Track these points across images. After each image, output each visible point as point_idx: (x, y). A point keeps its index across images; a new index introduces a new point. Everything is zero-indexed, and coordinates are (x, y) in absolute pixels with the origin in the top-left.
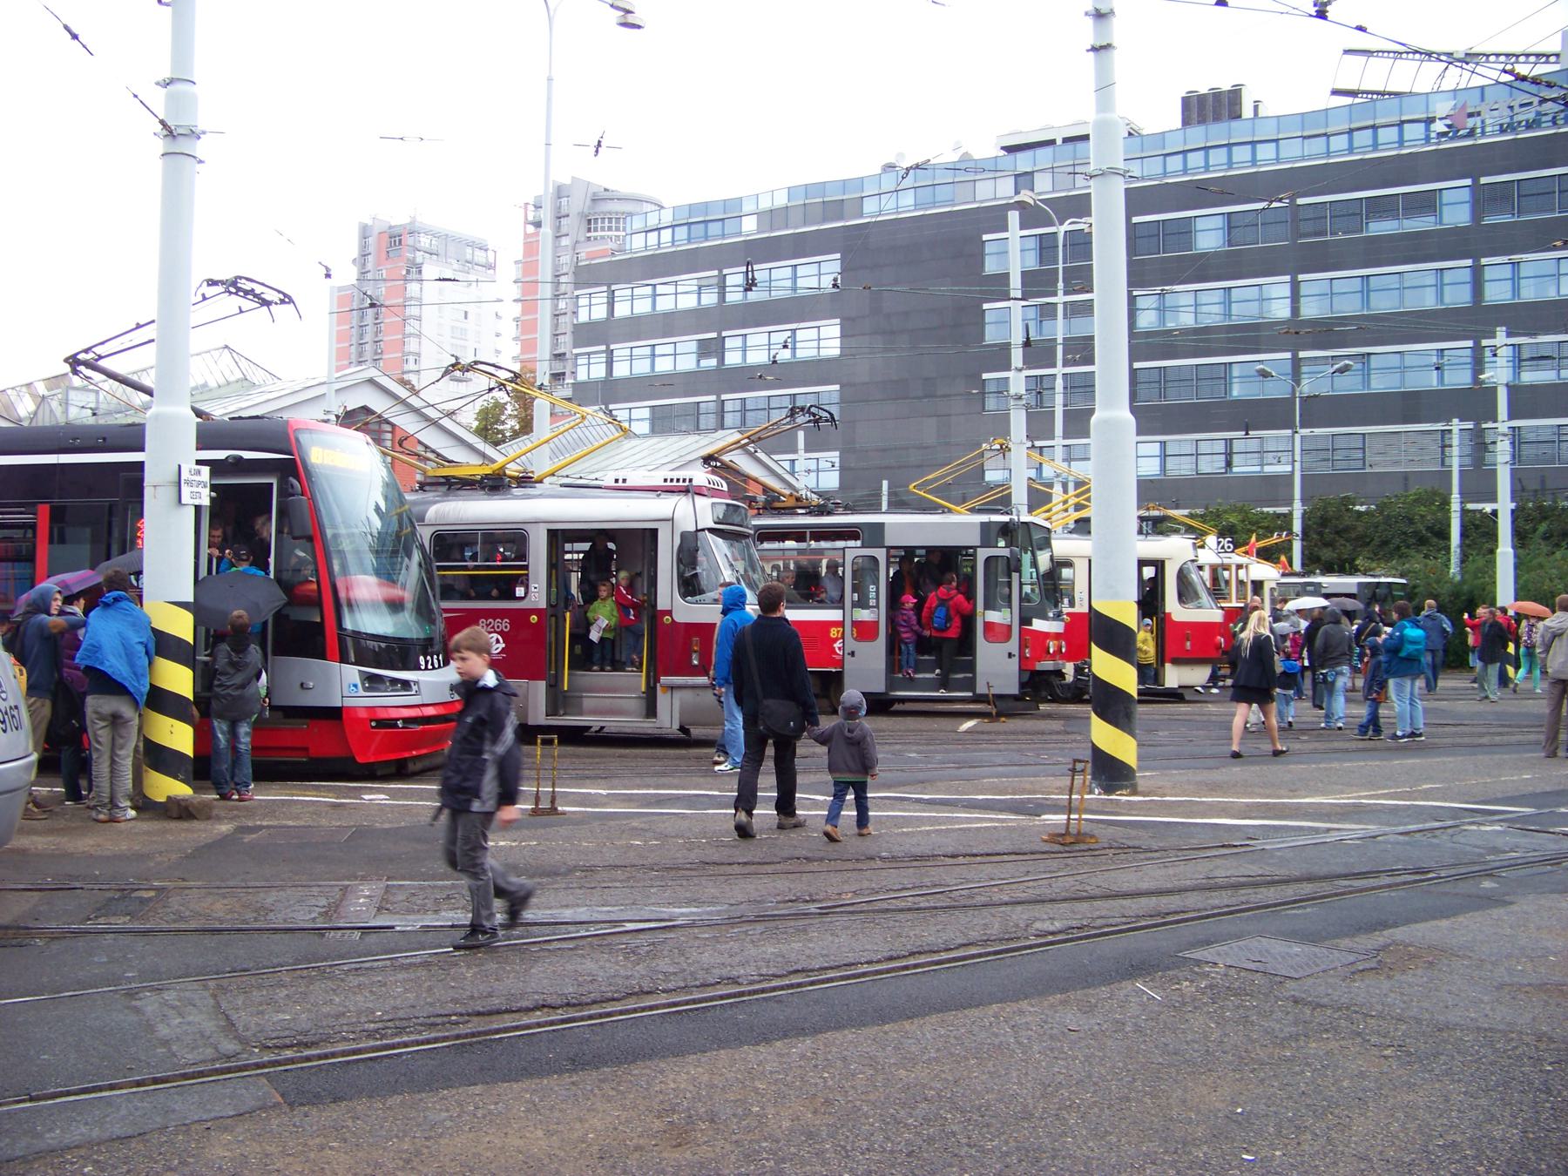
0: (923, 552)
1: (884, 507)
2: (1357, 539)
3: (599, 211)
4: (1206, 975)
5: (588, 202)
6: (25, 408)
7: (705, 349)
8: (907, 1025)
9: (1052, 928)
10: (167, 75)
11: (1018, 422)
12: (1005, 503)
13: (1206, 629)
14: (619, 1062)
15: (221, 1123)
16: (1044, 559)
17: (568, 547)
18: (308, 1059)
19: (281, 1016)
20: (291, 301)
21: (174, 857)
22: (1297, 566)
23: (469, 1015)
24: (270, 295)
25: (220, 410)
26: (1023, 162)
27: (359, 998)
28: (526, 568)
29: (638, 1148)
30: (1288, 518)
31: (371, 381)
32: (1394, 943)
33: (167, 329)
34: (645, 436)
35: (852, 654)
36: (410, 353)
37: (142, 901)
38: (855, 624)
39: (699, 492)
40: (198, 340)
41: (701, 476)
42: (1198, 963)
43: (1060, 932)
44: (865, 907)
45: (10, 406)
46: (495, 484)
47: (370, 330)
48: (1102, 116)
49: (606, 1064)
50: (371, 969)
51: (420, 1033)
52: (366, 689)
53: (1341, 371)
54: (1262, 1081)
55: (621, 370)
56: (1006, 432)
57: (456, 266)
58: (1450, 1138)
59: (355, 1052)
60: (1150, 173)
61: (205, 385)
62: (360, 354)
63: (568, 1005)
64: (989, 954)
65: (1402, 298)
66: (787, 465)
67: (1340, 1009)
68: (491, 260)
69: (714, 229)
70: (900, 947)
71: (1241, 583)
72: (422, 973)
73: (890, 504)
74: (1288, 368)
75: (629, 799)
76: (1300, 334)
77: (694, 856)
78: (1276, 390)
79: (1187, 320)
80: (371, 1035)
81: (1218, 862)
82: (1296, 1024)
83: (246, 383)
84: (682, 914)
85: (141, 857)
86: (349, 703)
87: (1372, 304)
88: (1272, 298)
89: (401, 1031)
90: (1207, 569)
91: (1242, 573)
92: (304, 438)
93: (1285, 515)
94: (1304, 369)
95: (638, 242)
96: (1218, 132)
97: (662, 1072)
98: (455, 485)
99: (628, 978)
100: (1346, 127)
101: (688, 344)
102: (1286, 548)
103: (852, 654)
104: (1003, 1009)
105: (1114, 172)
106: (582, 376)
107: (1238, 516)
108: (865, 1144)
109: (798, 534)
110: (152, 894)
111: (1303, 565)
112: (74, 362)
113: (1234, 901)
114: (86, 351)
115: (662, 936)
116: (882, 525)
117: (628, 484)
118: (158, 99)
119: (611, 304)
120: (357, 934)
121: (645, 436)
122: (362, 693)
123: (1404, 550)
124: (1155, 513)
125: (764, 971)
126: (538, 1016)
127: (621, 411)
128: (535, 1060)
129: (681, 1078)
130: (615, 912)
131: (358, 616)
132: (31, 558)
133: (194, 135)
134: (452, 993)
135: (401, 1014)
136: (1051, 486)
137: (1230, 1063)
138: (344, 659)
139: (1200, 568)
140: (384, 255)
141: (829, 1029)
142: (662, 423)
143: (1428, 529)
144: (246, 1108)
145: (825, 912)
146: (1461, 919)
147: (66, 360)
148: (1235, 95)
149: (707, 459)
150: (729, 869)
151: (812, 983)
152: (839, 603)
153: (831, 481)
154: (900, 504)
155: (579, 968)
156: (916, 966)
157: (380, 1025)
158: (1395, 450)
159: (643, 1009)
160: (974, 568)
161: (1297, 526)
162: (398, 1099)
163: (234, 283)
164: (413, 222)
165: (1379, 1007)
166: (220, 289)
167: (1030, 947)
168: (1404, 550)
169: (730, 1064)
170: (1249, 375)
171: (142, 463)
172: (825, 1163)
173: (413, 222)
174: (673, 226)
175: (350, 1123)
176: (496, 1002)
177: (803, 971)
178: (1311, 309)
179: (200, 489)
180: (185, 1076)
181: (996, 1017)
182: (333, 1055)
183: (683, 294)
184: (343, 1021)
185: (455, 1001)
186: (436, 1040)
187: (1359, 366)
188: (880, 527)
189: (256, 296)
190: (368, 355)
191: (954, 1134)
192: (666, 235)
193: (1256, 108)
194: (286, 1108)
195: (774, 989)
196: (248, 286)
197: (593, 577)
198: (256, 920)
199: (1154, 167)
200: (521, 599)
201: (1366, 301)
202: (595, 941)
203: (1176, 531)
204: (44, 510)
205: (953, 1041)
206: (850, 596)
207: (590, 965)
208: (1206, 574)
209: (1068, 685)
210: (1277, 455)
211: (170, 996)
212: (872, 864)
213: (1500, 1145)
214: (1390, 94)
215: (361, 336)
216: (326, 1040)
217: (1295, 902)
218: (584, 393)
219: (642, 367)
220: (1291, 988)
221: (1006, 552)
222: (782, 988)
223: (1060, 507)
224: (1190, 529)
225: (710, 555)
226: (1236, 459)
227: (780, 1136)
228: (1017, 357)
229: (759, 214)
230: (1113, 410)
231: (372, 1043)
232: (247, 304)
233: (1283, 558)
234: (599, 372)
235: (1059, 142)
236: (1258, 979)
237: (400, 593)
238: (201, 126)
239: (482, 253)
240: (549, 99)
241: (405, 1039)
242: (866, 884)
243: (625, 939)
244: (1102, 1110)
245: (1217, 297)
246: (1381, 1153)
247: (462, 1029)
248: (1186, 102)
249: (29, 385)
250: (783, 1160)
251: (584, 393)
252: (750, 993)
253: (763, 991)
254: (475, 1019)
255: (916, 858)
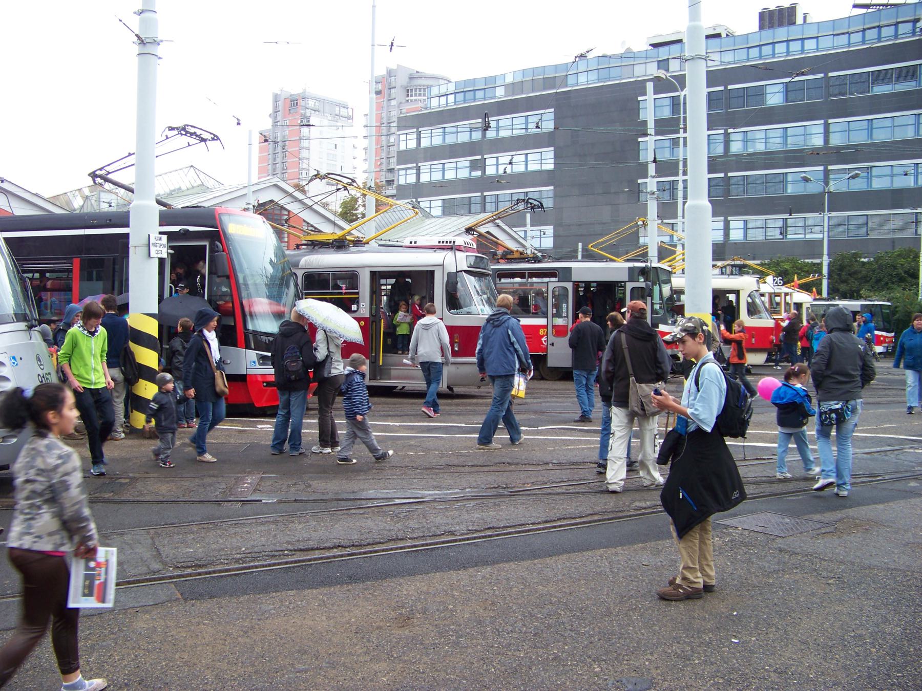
0: (595, 284)
1: (580, 258)
2: (861, 278)
3: (415, 84)
4: (730, 534)
5: (407, 80)
6: (77, 203)
7: (474, 166)
8: (548, 560)
9: (644, 505)
10: (140, 8)
11: (652, 208)
12: (644, 256)
13: (765, 331)
14: (376, 579)
15: (145, 609)
16: (666, 290)
17: (383, 281)
18: (199, 574)
19: (188, 550)
20: (218, 139)
21: (144, 459)
22: (825, 294)
23: (295, 550)
24: (205, 136)
25: (179, 204)
26: (663, 53)
27: (234, 540)
28: (358, 293)
29: (379, 628)
30: (820, 264)
31: (276, 186)
32: (847, 517)
33: (141, 156)
34: (438, 217)
35: (553, 344)
36: (303, 169)
37: (122, 485)
38: (554, 326)
39: (459, 249)
40: (160, 166)
41: (460, 241)
42: (726, 527)
43: (649, 508)
44: (538, 492)
45: (69, 202)
46: (340, 245)
47: (280, 155)
48: (693, 23)
49: (369, 580)
50: (244, 524)
51: (265, 560)
52: (260, 364)
53: (853, 177)
54: (752, 596)
55: (425, 178)
56: (645, 215)
57: (330, 118)
58: (859, 632)
59: (227, 571)
60: (730, 60)
61: (180, 189)
62: (274, 170)
63: (353, 545)
64: (605, 520)
65: (893, 132)
66: (522, 234)
67: (806, 556)
68: (350, 114)
69: (480, 94)
70: (552, 515)
71: (787, 304)
72: (273, 526)
73: (583, 257)
74: (822, 177)
75: (412, 428)
76: (828, 155)
77: (442, 461)
78: (814, 188)
79: (760, 147)
80: (237, 561)
81: (752, 468)
82: (778, 563)
83: (203, 189)
84: (430, 495)
85: (127, 460)
86: (250, 372)
87: (874, 137)
88: (811, 134)
89: (254, 559)
90: (767, 295)
91: (788, 298)
92: (225, 219)
93: (818, 264)
94: (831, 176)
95: (434, 103)
96: (782, 33)
97: (400, 585)
98: (317, 245)
99: (390, 531)
100: (861, 27)
101: (465, 162)
102: (818, 284)
103: (553, 344)
104: (606, 552)
105: (699, 57)
106: (402, 181)
107: (788, 265)
108: (510, 628)
109: (521, 274)
110: (127, 480)
111: (828, 294)
112: (94, 175)
113: (757, 491)
114: (101, 169)
115: (414, 507)
116: (570, 269)
117: (417, 244)
118: (135, 23)
119: (419, 139)
120: (240, 504)
121: (438, 217)
122: (258, 366)
123: (890, 285)
124: (738, 263)
125: (470, 528)
126: (335, 552)
127: (424, 203)
128: (329, 577)
129: (410, 589)
130: (390, 493)
131: (256, 321)
132: (69, 289)
133: (156, 42)
134: (287, 539)
135: (256, 550)
136: (675, 246)
137: (734, 586)
138: (248, 347)
139: (762, 295)
140: (288, 112)
141: (503, 561)
142: (449, 209)
143: (905, 272)
144: (160, 601)
145: (513, 494)
146: (891, 504)
147: (89, 175)
148: (792, 10)
149: (469, 230)
150: (462, 469)
151: (498, 535)
152: (545, 315)
153: (548, 243)
154: (589, 256)
155: (363, 525)
156: (560, 526)
157: (243, 556)
158: (886, 225)
159: (397, 549)
160: (624, 294)
161: (825, 271)
162: (246, 597)
163: (184, 129)
164: (304, 92)
165: (830, 555)
166: (176, 132)
167: (630, 516)
168: (890, 285)
169: (439, 581)
170: (798, 180)
171: (128, 234)
172: (485, 638)
173: (304, 92)
174: (455, 93)
175: (217, 610)
176: (311, 544)
177: (493, 528)
178: (836, 140)
179: (161, 248)
180: (129, 583)
181: (601, 556)
182: (214, 572)
183: (463, 132)
184: (222, 553)
185: (288, 543)
186: (274, 565)
187: (865, 174)
188: (569, 270)
189: (197, 136)
190: (279, 171)
191: (563, 623)
192: (451, 98)
193: (805, 18)
194: (182, 601)
195: (475, 538)
196: (192, 130)
197: (396, 298)
198: (184, 496)
199: (742, 55)
200: (355, 312)
201: (870, 135)
202: (376, 510)
203: (748, 273)
204: (77, 262)
205: (573, 569)
206: (551, 310)
207: (370, 523)
208: (766, 299)
209: (681, 364)
210: (814, 228)
211: (127, 538)
212: (547, 467)
213: (888, 637)
214: (891, 5)
215: (275, 159)
216: (212, 563)
217: (793, 492)
218: (403, 192)
219: (437, 176)
220: (779, 543)
221: (643, 285)
222: (479, 538)
223: (681, 257)
224: (755, 272)
225: (465, 285)
226: (790, 231)
227: (461, 621)
228: (652, 169)
229: (506, 86)
230: (698, 200)
231: (237, 566)
232: (192, 141)
233: (814, 290)
234: (412, 179)
235: (724, 35)
236: (761, 537)
237: (282, 309)
238: (160, 37)
239: (345, 110)
240: (374, 18)
241: (257, 564)
242: (540, 478)
243: (393, 508)
244: (653, 611)
245: (779, 133)
246: (815, 640)
247: (290, 559)
248: (762, 15)
249: (80, 190)
250: (461, 636)
251: (403, 192)
252: (460, 540)
253: (468, 539)
254: (298, 553)
255: (573, 464)
